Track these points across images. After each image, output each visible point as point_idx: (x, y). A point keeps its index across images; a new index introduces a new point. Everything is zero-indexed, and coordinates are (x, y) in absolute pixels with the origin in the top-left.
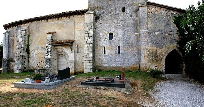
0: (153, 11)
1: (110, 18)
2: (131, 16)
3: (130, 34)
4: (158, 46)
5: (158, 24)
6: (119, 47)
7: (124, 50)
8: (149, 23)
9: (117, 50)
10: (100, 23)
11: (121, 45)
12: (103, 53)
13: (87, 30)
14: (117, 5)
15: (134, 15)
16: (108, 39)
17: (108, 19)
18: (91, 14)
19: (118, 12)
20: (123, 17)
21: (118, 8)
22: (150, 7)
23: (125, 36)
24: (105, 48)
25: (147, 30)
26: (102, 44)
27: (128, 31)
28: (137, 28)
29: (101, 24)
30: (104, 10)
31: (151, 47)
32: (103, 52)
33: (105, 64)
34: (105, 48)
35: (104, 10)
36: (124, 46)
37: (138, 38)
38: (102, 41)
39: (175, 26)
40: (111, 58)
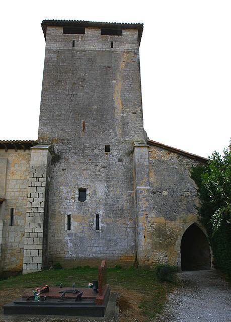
0: (158, 156)
1: (82, 160)
2: (120, 160)
3: (118, 191)
4: (168, 216)
5: (167, 178)
6: (97, 216)
7: (107, 224)
8: (152, 174)
9: (95, 222)
10: (61, 168)
11: (101, 213)
12: (66, 228)
13: (34, 180)
14: (94, 140)
15: (126, 160)
16: (77, 199)
17: (78, 161)
18: (44, 151)
19: (96, 151)
20: (105, 161)
21: (97, 146)
22: (153, 149)
23: (109, 195)
24: (69, 216)
25: (148, 187)
26: (65, 208)
27: (115, 186)
28: (131, 182)
29: (63, 170)
30: (70, 146)
31: (156, 217)
32: (66, 226)
33: (70, 253)
34: (69, 216)
35: (70, 146)
36: (107, 214)
37: (134, 201)
38: (64, 203)
39: (193, 182)
40: (81, 239)
